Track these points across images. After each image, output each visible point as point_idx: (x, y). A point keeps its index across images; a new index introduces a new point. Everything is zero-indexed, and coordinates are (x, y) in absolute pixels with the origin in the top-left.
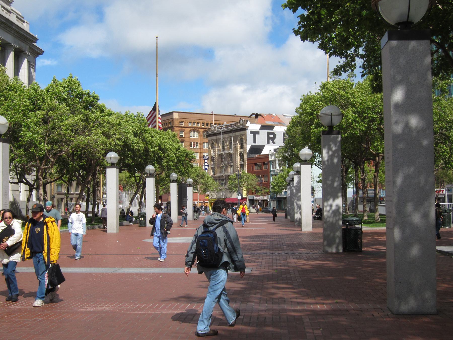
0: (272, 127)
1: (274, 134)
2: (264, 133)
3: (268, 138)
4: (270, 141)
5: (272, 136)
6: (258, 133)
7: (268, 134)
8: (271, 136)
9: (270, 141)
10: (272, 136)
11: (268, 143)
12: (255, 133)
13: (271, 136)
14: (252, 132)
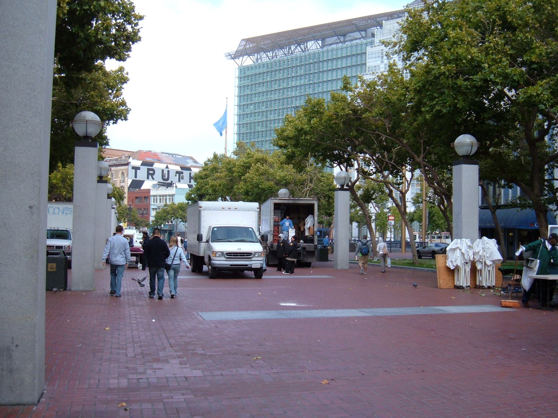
0: (152, 164)
1: (153, 170)
2: (144, 169)
3: (148, 174)
4: (150, 176)
5: (152, 172)
6: (139, 168)
7: (148, 170)
8: (150, 172)
9: (150, 176)
10: (152, 172)
11: (148, 178)
12: (136, 169)
13: (150, 172)
14: (133, 168)
